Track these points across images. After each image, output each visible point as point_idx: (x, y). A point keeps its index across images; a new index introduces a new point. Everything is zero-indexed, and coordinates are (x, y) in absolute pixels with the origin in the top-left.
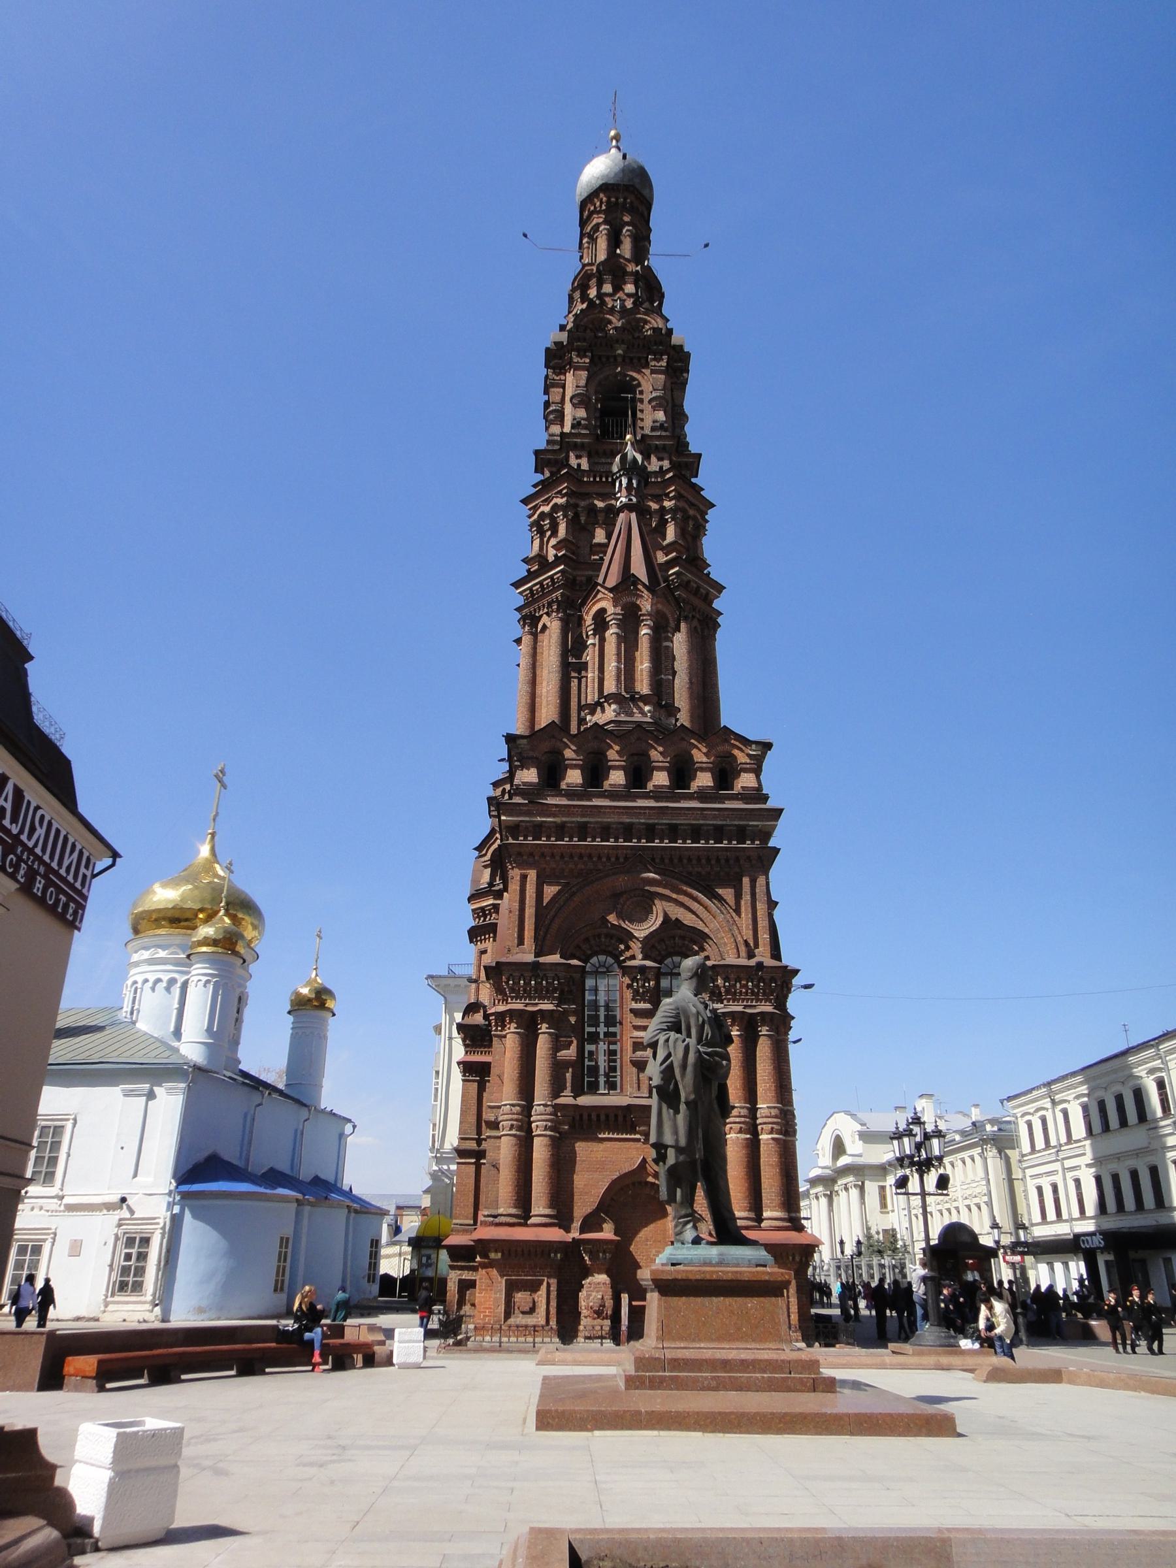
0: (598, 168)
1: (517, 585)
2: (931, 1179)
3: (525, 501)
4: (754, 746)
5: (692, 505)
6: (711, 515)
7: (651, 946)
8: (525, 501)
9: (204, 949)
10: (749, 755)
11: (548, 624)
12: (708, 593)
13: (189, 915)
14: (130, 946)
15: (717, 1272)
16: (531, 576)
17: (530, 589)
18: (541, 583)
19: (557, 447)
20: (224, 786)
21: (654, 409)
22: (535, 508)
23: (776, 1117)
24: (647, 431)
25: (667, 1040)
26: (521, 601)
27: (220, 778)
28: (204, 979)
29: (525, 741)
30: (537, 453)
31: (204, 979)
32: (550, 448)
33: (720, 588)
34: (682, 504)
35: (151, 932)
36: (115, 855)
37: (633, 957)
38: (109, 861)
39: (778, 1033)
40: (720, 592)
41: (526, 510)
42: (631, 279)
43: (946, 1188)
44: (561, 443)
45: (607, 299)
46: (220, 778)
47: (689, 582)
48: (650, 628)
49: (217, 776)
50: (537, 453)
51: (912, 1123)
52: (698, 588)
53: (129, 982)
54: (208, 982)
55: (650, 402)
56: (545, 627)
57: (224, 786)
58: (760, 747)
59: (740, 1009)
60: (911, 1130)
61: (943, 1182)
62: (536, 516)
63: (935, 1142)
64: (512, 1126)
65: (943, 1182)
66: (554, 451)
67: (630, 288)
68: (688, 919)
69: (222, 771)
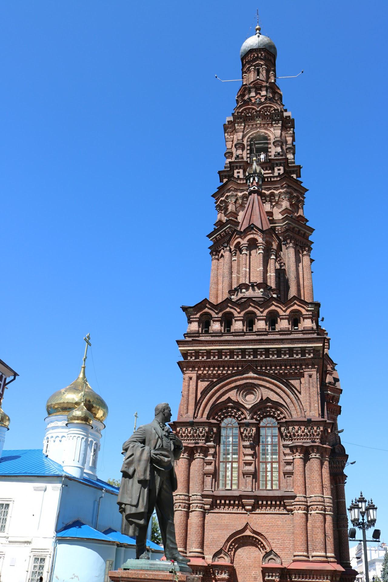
0: (253, 41)
1: (209, 236)
2: (370, 533)
3: (213, 196)
4: (310, 306)
5: (295, 190)
6: (306, 195)
7: (254, 410)
8: (213, 196)
9: (76, 421)
10: (307, 311)
11: (224, 254)
12: (305, 233)
13: (70, 406)
14: (47, 420)
15: (144, 574)
16: (216, 231)
17: (215, 237)
18: (220, 234)
19: (229, 169)
20: (89, 344)
21: (276, 146)
22: (217, 199)
23: (330, 503)
24: (273, 157)
25: (133, 447)
26: (212, 243)
27: (88, 341)
28: (82, 436)
29: (192, 309)
30: (219, 172)
31: (82, 436)
32: (226, 170)
33: (312, 230)
34: (289, 190)
35: (55, 414)
36: (15, 375)
37: (245, 418)
38: (12, 378)
39: (322, 457)
40: (312, 232)
41: (214, 200)
42: (265, 89)
43: (378, 538)
44: (230, 167)
45: (252, 99)
46: (88, 341)
47: (294, 228)
48: (263, 250)
49: (85, 339)
50: (219, 172)
51: (359, 501)
52: (299, 230)
53: (45, 438)
54: (83, 438)
55: (274, 143)
56: (222, 256)
57: (89, 344)
58: (313, 306)
59: (300, 444)
60: (358, 505)
61: (377, 534)
62: (218, 203)
63: (371, 511)
64: (180, 505)
65: (377, 534)
66: (227, 171)
67: (264, 93)
68: (274, 398)
69: (88, 337)
